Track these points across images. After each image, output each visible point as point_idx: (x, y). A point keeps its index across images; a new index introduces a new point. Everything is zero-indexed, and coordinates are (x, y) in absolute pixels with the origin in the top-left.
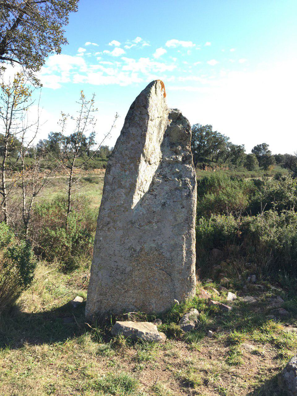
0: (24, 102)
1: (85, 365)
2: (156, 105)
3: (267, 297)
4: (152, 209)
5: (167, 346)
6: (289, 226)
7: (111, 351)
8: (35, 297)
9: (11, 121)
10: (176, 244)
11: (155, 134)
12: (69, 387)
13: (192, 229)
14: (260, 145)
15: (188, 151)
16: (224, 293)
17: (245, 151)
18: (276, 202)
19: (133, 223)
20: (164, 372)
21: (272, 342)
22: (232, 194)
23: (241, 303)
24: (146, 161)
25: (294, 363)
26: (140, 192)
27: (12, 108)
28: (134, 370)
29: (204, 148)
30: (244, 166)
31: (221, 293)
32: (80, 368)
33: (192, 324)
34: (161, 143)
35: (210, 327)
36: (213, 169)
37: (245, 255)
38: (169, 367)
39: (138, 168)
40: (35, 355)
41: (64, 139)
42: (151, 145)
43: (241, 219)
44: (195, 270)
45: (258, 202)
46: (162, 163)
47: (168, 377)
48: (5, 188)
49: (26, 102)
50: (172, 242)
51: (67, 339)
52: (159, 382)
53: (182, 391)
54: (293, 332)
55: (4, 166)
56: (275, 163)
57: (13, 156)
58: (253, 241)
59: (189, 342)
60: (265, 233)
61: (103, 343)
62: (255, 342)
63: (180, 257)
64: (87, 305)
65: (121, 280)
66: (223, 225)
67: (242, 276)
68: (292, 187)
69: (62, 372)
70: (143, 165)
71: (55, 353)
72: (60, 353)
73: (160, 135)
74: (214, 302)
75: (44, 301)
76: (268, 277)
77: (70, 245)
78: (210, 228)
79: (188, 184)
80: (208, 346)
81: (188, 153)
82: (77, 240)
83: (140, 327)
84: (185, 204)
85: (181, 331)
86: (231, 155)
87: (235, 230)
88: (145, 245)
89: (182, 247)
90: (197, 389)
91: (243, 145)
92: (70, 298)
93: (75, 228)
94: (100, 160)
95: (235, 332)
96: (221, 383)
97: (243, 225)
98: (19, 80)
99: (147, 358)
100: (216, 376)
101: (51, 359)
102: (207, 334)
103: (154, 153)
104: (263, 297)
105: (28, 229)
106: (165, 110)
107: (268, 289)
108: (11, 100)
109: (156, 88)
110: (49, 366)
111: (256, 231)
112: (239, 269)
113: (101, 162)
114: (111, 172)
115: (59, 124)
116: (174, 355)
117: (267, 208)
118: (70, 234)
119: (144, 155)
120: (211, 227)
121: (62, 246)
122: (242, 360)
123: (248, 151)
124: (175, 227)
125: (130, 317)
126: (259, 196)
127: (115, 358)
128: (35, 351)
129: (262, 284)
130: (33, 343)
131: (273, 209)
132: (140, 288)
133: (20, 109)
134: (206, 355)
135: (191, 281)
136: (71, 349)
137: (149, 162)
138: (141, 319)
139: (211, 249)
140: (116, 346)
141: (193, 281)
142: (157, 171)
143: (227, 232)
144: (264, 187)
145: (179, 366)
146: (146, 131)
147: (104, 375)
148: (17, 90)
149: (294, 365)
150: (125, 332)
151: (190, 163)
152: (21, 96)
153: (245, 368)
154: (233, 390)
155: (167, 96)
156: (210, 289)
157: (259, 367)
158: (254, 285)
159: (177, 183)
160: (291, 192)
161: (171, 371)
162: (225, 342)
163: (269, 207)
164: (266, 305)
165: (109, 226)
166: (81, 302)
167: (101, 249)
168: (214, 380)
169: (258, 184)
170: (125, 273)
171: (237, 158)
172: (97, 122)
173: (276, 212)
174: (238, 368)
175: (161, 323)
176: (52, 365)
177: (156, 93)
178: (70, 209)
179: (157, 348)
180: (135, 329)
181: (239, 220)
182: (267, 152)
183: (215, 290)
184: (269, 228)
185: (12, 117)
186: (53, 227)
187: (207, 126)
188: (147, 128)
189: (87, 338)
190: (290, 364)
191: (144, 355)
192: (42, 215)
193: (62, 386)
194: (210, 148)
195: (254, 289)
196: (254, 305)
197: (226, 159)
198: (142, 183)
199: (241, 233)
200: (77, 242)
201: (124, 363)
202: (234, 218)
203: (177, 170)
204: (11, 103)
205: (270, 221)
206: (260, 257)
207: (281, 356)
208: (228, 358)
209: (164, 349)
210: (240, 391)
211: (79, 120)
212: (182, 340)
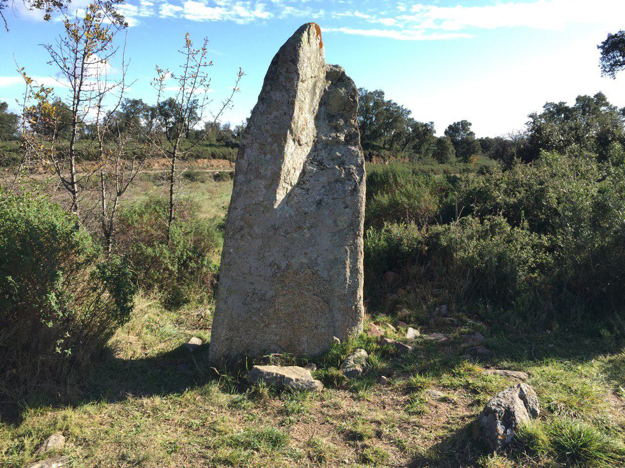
0: (101, 50)
1: (215, 419)
2: (309, 59)
3: (462, 333)
4: (304, 209)
5: (325, 396)
6: (494, 238)
7: (248, 402)
8: (132, 338)
9: (82, 80)
10: (336, 259)
11: (307, 101)
12: (196, 444)
13: (359, 238)
14: (458, 123)
15: (354, 127)
16: (402, 329)
17: (435, 133)
18: (478, 204)
19: (275, 229)
20: (323, 426)
21: (467, 386)
22: (415, 194)
23: (426, 342)
24: (294, 140)
25: (493, 405)
26: (286, 185)
27: (83, 60)
28: (281, 424)
29: (371, 126)
30: (433, 156)
31: (398, 330)
32: (208, 423)
33: (359, 368)
34: (315, 115)
35: (383, 372)
36: (385, 161)
37: (432, 279)
38: (329, 419)
39: (283, 150)
40: (143, 410)
41: (148, 111)
42: (302, 119)
43: (427, 230)
44: (362, 296)
45: (452, 206)
46: (316, 143)
47: (328, 431)
48: (75, 183)
49: (104, 50)
50: (331, 257)
51: (185, 390)
52: (316, 437)
53: (347, 445)
54: (495, 374)
55: (73, 149)
56: (481, 152)
57: (64, 137)
58: (443, 261)
59: (355, 390)
60: (461, 248)
61: (237, 394)
62: (444, 387)
63: (342, 277)
64: (210, 348)
65: (259, 310)
66: (401, 237)
67: (428, 307)
68: (500, 184)
69: (183, 429)
70: (290, 147)
71: (170, 407)
72: (178, 406)
73: (314, 103)
74: (389, 340)
75: (145, 344)
76: (464, 308)
77: (175, 269)
78: (382, 242)
79: (354, 174)
80: (380, 395)
81: (354, 129)
82: (185, 262)
83: (287, 373)
84: (349, 203)
85: (343, 378)
86: (413, 139)
87: (418, 245)
88: (293, 260)
89: (345, 264)
90: (367, 442)
91: (432, 123)
92: (183, 340)
93: (182, 243)
94: (207, 146)
95: (418, 376)
96: (399, 434)
97: (430, 237)
98: (92, 16)
99: (298, 410)
100: (393, 427)
101: (167, 414)
102: (380, 381)
103: (306, 129)
104: (457, 334)
105: (111, 245)
106: (321, 67)
107: (463, 323)
108: (81, 46)
109: (309, 34)
110: (165, 422)
111: (448, 246)
112: (424, 299)
113: (208, 148)
114: (245, 155)
115: (153, 84)
116: (334, 406)
117: (465, 214)
118: (174, 252)
119: (292, 132)
120: (384, 241)
121: (164, 270)
122: (426, 408)
123: (439, 132)
124: (335, 235)
125: (273, 360)
126: (454, 197)
127: (254, 411)
128: (143, 405)
129: (456, 317)
130: (138, 394)
131: (473, 215)
132: (285, 321)
133: (96, 61)
134: (378, 406)
135: (357, 311)
136: (192, 401)
137: (299, 141)
138: (287, 363)
139: (385, 272)
140: (255, 396)
141: (360, 311)
142: (309, 155)
143: (407, 246)
144: (460, 183)
145: (343, 418)
146: (295, 96)
147: (242, 430)
148: (90, 33)
149: (493, 408)
150: (267, 379)
151: (355, 144)
152: (95, 42)
153: (430, 417)
154: (414, 442)
155: (324, 47)
156: (384, 324)
157: (449, 416)
158: (445, 319)
159: (338, 172)
160: (499, 190)
161: (332, 424)
162: (404, 389)
163: (468, 211)
164: (460, 343)
165: (243, 232)
166: (200, 344)
167: (231, 265)
168: (390, 431)
169: (453, 181)
170: (265, 300)
171: (422, 143)
172: (211, 83)
173: (477, 219)
174: (422, 418)
175: (316, 369)
176: (169, 420)
177: (309, 41)
178: (173, 215)
179: (312, 398)
180: (280, 375)
181: (425, 230)
182: (468, 134)
183: (390, 325)
184: (466, 241)
185: (84, 74)
186: (150, 244)
187: (376, 92)
188: (296, 92)
189: (214, 388)
190: (489, 406)
191: (294, 407)
192: (133, 223)
193: (186, 443)
194: (380, 127)
195: (444, 324)
196: (443, 344)
197: (405, 145)
198: (289, 171)
199: (426, 248)
200: (185, 265)
201: (268, 417)
202: (417, 228)
203: (338, 154)
204: (81, 52)
205: (468, 231)
206: (453, 280)
207: (478, 402)
208: (409, 407)
209: (320, 399)
210: (423, 443)
211: (184, 79)
212: (344, 389)
